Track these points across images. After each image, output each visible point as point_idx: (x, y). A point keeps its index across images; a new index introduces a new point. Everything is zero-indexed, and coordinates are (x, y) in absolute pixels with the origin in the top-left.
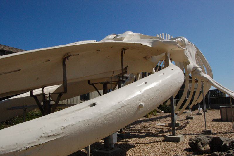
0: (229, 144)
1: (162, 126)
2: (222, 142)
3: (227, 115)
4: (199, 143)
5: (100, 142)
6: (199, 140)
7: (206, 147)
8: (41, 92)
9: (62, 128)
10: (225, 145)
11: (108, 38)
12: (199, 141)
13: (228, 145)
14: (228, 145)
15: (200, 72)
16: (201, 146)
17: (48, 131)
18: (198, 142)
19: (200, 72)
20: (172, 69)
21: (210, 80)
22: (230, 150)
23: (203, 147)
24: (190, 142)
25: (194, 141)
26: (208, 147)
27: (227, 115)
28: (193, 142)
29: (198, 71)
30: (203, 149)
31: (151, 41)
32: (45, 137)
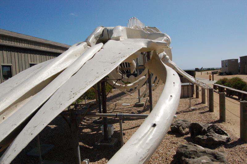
0: (207, 128)
1: (128, 107)
2: (201, 127)
3: (188, 94)
4: (180, 128)
5: (87, 132)
6: (180, 125)
7: (185, 130)
8: (123, 125)
9: (148, 150)
10: (205, 130)
11: (98, 31)
12: (180, 126)
13: (206, 129)
14: (206, 129)
15: (168, 59)
16: (183, 130)
17: (142, 156)
18: (179, 127)
19: (168, 59)
20: (174, 75)
21: (176, 67)
22: (208, 133)
23: (184, 130)
24: (172, 126)
25: (175, 125)
26: (187, 130)
27: (188, 94)
28: (175, 126)
29: (166, 58)
30: (184, 132)
31: (147, 42)
32: (142, 161)
